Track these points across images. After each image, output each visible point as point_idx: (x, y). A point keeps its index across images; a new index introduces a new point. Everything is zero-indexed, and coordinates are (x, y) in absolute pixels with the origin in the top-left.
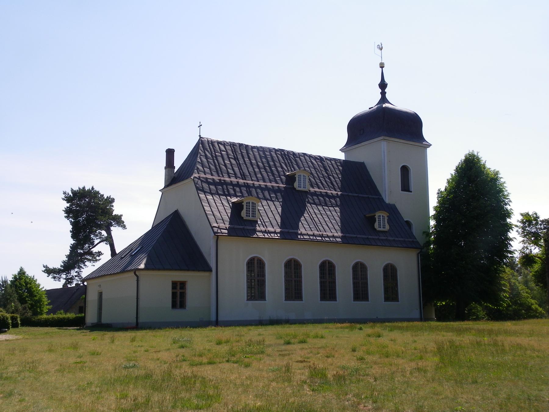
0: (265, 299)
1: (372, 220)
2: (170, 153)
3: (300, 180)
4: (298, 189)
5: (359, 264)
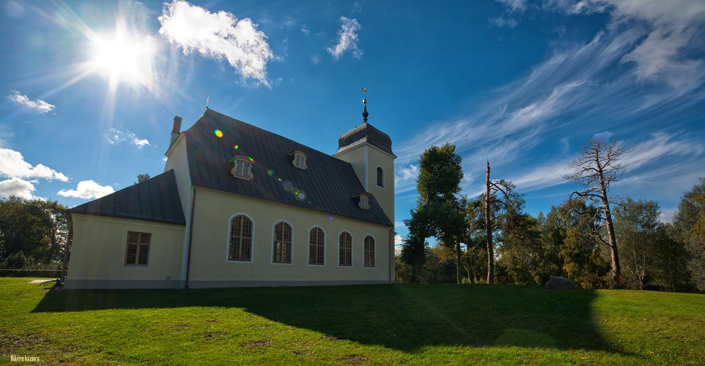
2: (178, 121)
3: (298, 160)
4: (296, 166)
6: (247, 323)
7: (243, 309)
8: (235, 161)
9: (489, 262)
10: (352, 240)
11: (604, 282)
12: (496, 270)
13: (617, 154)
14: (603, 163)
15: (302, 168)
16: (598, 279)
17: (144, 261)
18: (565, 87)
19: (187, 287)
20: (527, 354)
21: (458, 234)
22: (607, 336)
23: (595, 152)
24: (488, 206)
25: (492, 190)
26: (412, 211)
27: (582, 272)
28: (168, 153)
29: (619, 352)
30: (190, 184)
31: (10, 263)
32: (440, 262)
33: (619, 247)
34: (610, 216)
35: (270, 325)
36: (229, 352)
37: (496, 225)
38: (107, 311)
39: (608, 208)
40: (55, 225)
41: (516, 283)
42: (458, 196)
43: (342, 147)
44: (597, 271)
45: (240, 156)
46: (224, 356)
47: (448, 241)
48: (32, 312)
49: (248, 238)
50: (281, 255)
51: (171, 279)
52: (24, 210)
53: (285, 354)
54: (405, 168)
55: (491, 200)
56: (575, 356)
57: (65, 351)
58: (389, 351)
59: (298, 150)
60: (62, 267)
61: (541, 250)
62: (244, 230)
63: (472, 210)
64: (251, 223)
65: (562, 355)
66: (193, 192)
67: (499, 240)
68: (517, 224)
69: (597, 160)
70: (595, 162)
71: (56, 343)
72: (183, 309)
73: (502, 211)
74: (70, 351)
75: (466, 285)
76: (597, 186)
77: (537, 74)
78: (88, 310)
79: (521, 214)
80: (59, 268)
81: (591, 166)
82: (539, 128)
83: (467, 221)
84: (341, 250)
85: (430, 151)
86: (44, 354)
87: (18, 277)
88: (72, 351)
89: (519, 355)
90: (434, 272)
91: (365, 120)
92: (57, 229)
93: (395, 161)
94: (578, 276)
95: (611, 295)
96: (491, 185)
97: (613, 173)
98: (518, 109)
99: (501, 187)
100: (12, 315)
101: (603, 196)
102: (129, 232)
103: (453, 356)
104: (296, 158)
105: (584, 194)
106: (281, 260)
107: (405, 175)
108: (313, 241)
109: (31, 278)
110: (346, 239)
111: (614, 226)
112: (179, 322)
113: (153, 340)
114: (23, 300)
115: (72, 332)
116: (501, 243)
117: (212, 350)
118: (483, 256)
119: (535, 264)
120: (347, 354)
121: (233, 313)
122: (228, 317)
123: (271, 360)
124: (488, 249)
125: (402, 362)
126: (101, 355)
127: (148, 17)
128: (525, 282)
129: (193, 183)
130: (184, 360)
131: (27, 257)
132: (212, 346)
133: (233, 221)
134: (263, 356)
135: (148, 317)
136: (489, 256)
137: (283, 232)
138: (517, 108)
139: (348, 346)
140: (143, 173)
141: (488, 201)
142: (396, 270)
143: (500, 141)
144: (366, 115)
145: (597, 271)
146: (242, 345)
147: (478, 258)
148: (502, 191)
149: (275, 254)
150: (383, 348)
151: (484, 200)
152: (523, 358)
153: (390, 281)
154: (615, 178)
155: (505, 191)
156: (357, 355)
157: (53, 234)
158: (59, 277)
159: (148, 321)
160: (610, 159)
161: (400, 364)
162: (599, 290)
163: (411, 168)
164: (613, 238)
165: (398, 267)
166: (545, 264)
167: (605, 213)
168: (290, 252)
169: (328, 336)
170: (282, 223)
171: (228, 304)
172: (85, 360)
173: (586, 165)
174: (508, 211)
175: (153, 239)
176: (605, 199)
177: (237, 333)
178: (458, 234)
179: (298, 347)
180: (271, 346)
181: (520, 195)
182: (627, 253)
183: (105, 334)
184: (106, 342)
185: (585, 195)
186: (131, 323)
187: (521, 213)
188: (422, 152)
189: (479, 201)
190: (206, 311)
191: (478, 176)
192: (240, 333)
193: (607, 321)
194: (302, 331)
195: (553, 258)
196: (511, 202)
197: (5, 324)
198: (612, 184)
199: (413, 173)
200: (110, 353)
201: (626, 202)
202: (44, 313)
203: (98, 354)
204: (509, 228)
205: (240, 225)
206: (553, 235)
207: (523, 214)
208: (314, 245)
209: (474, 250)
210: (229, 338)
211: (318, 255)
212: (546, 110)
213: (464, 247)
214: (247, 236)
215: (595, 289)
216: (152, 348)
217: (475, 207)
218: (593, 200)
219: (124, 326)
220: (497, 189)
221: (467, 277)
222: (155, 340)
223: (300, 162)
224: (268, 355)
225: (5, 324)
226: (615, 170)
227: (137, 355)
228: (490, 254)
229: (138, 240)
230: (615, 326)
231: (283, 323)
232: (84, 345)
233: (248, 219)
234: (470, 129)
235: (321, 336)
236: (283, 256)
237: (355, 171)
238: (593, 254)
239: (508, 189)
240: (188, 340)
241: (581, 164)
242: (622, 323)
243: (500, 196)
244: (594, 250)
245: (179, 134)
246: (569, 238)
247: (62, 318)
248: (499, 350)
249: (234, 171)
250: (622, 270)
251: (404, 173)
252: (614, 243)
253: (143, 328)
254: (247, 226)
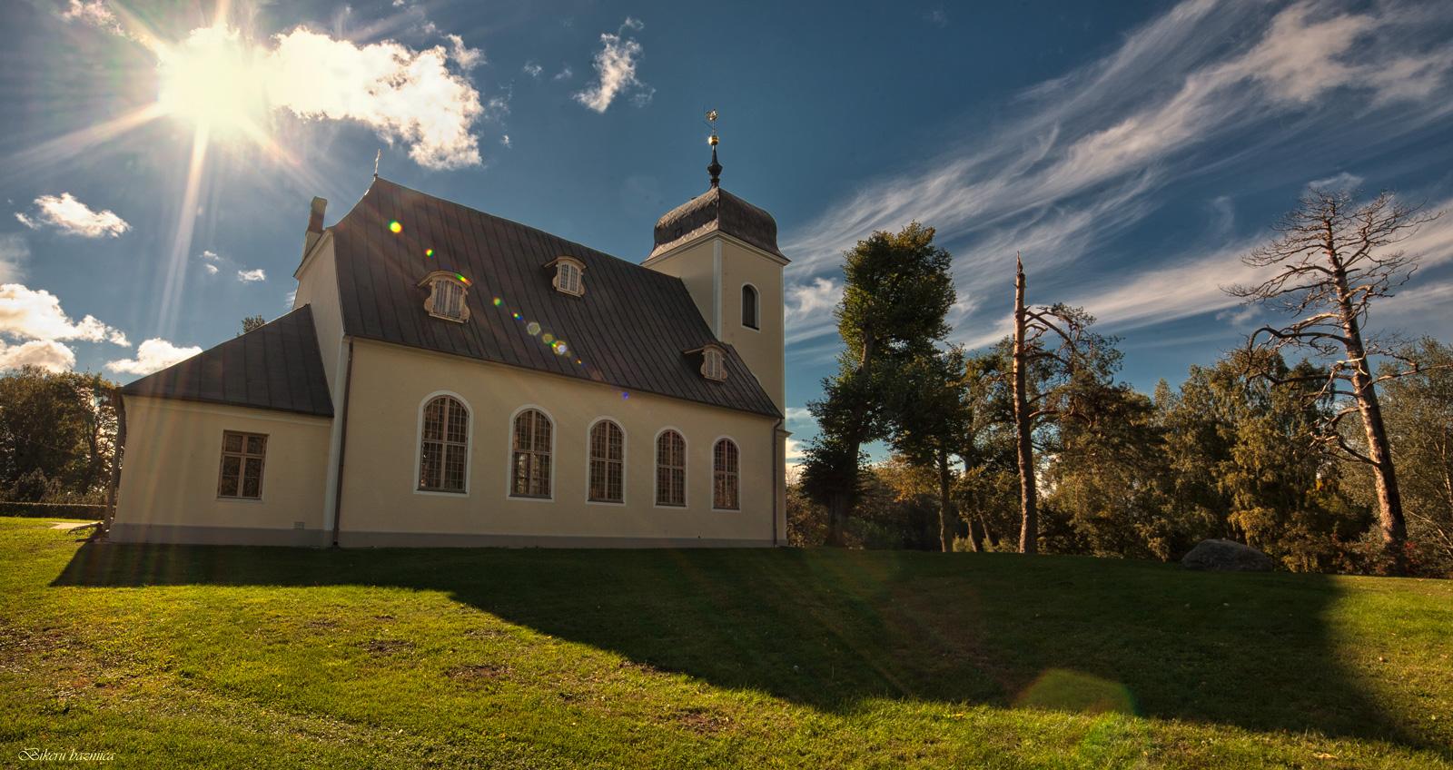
5: (726, 443)
6: (458, 625)
7: (449, 593)
8: (431, 284)
9: (1025, 500)
10: (739, 456)
11: (1356, 559)
12: (1044, 522)
13: (1389, 226)
14: (1346, 252)
15: (572, 293)
16: (1338, 549)
17: (253, 490)
18: (1218, 72)
19: (336, 543)
20: (1151, 734)
21: (943, 433)
22: (1390, 701)
23: (1324, 225)
24: (1021, 367)
25: (1031, 329)
26: (827, 381)
27: (1286, 531)
28: (299, 273)
29: (1433, 746)
30: (343, 334)
31: (23, 491)
32: (895, 501)
33: (1399, 467)
34: (1371, 386)
35: (506, 632)
36: (421, 687)
37: (1042, 413)
38: (183, 588)
39: (1364, 365)
40: (98, 419)
41: (1098, 554)
42: (943, 347)
43: (661, 243)
44: (1335, 529)
45: (441, 273)
46: (412, 694)
47: (916, 449)
48: (54, 584)
49: (458, 444)
50: (527, 479)
51: (306, 528)
52: (45, 391)
53: (541, 699)
54: (803, 287)
55: (1028, 355)
56: (1295, 750)
57: (106, 665)
58: (782, 706)
59: (564, 255)
60: (106, 498)
61: (1167, 476)
62: (450, 428)
63: (977, 379)
64: (464, 413)
65: (1255, 743)
66: (347, 350)
67: (1049, 447)
68: (1100, 410)
69: (1330, 246)
70: (1324, 250)
71: (91, 647)
72: (328, 589)
73: (1059, 381)
74: (115, 665)
75: (964, 554)
76: (1331, 313)
77: (1137, 47)
78: (150, 585)
79: (1110, 387)
80: (103, 502)
81: (1312, 261)
82: (1147, 177)
83: (966, 403)
84: (659, 470)
85: (870, 244)
86: (70, 669)
87: (33, 517)
88: (119, 666)
89: (1126, 736)
90: (883, 522)
91: (715, 182)
92: (99, 426)
93: (787, 271)
94: (1274, 540)
95: (1386, 593)
96: (1027, 317)
97: (1381, 278)
98: (1088, 136)
99: (1054, 320)
100: (20, 590)
101: (1348, 336)
102: (225, 431)
103: (945, 726)
104: (559, 272)
105: (1292, 332)
106: (527, 490)
107: (804, 302)
108: (597, 451)
109: (56, 519)
110: (671, 446)
111: (1383, 413)
112: (320, 616)
113: (268, 651)
114: (39, 560)
115: (121, 627)
116: (1054, 456)
117: (385, 681)
118: (1007, 488)
119: (1148, 506)
120: (682, 706)
121: (428, 603)
122: (418, 610)
123: (510, 711)
124: (1022, 471)
125: (815, 734)
126: (171, 677)
127: (258, 11)
128: (1121, 551)
129: (349, 332)
130: (330, 699)
131: (49, 480)
132: (386, 670)
133: (428, 408)
134: (492, 699)
135: (261, 603)
136: (1024, 487)
137: (532, 431)
138: (1087, 133)
139: (685, 687)
140: (253, 316)
141: (1020, 357)
142: (788, 517)
143: (1043, 212)
144: (715, 170)
145: (1335, 529)
146: (447, 673)
147: (993, 491)
148: (1058, 331)
149: (516, 478)
150: (768, 699)
151: (1010, 354)
152: (1140, 744)
153: (775, 541)
154: (1385, 290)
155: (1066, 330)
156: (707, 711)
157: (94, 437)
158: (102, 519)
159: (259, 611)
160: (1368, 242)
161: (810, 736)
162: (1343, 577)
163: (817, 286)
164: (1382, 442)
165: (793, 511)
166: (1175, 508)
167: (1355, 380)
168: (547, 475)
169: (636, 663)
170: (530, 413)
171: (418, 584)
172: (141, 685)
173: (1295, 260)
174: (1076, 379)
176: (1355, 344)
177: (437, 646)
178: (943, 433)
179: (568, 683)
180: (509, 678)
181: (1108, 341)
182: (1424, 482)
183: (180, 635)
184: (181, 652)
185: (1293, 336)
186: (227, 615)
187: (1110, 383)
188: (851, 247)
189: (994, 357)
190: (372, 595)
191: (985, 298)
192: (444, 646)
193: (1385, 661)
194: (576, 649)
195: (1199, 492)
196: (1081, 356)
197: (8, 606)
198: (1376, 304)
199: (823, 296)
200: (187, 675)
201: (1420, 350)
202: (74, 589)
203: (166, 675)
204: (1075, 423)
205: (442, 418)
206: (1199, 438)
207: (1116, 384)
208: (601, 459)
209: (983, 474)
210: (421, 656)
211: (610, 482)
212: (1165, 132)
213: (957, 465)
214: (456, 440)
215: (1325, 572)
216: (266, 668)
217: (986, 371)
218: (1316, 347)
219: (214, 620)
220: (1044, 326)
221: (964, 535)
222: (273, 652)
223: (569, 279)
224: (504, 697)
225: (8, 606)
226: (1385, 270)
227: (237, 681)
228: (1026, 483)
229: (243, 448)
230: (1411, 675)
231: (534, 629)
232: (139, 654)
234: (962, 191)
235: (619, 662)
236: (533, 483)
237: (691, 295)
238: (1319, 485)
239: (1074, 325)
240: (337, 656)
241: (1278, 258)
242: (1433, 667)
243: (1051, 342)
244: (1318, 476)
245: (321, 232)
246: (1245, 443)
247: (104, 598)
248: (1070, 719)
249: (429, 304)
250: (1412, 527)
251: (799, 297)
252: (1385, 456)
253: (251, 625)
254: (457, 419)
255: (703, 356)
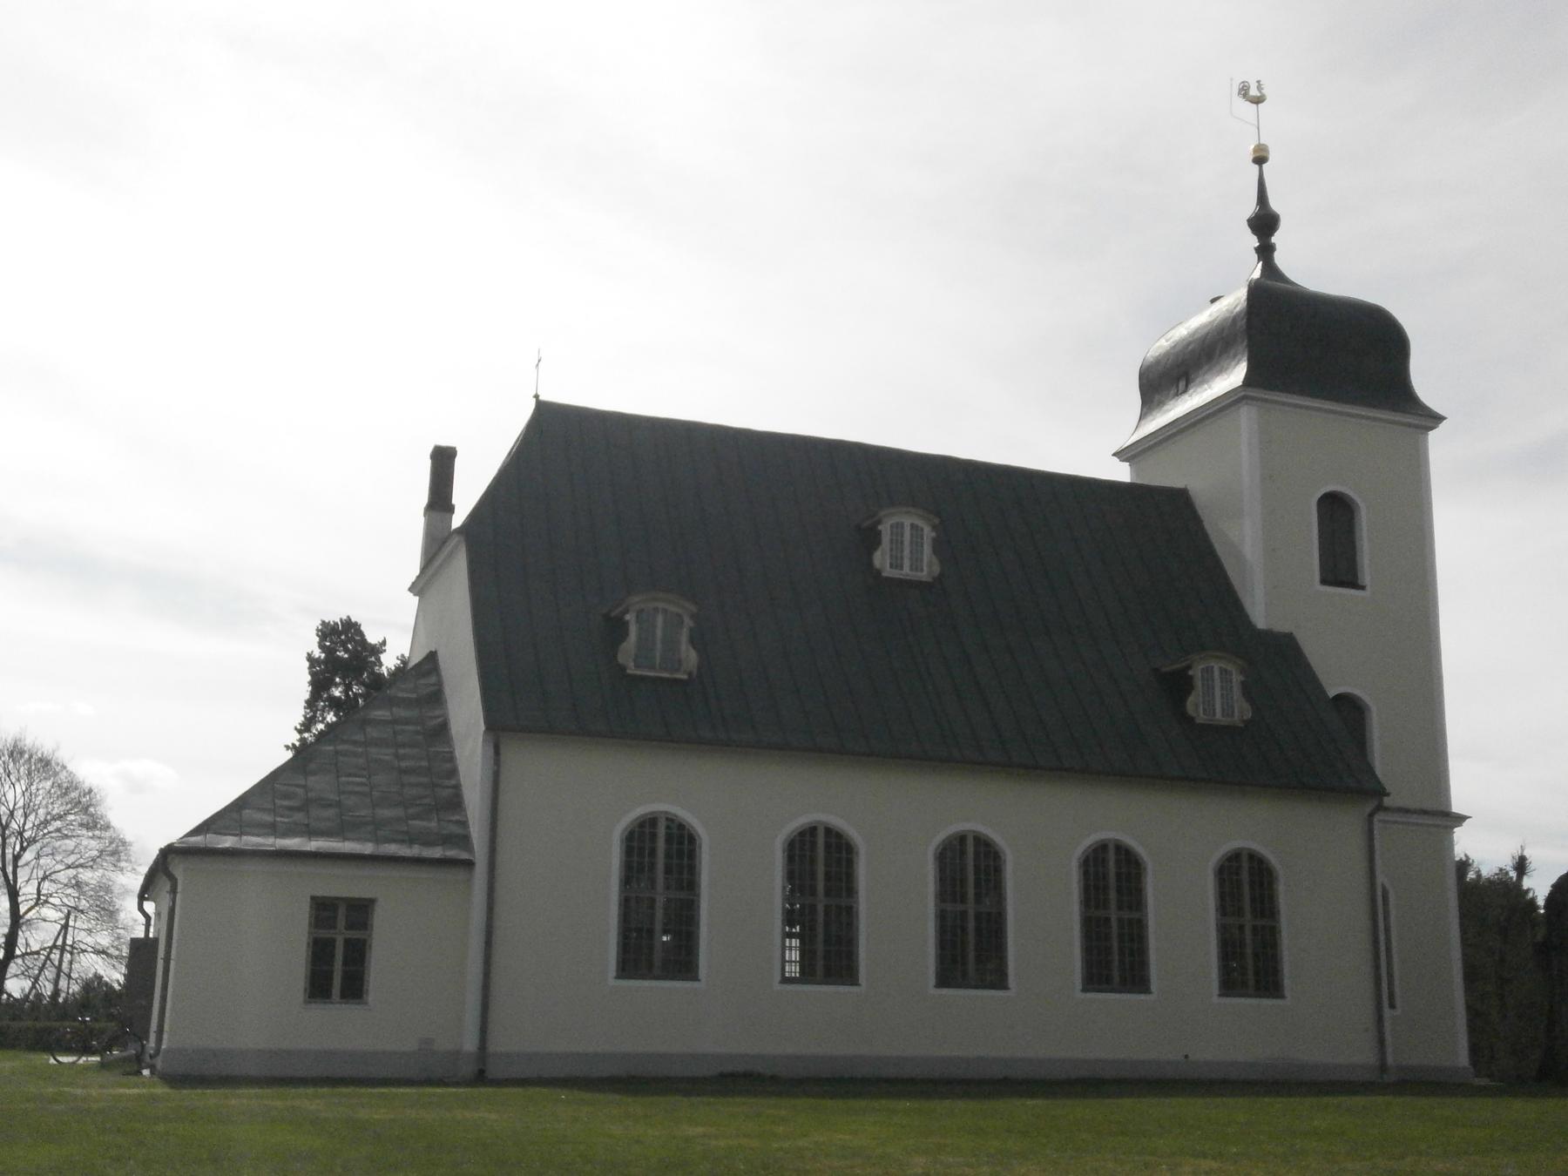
0: (697, 972)
1: (1178, 686)
2: (443, 461)
3: (897, 542)
4: (888, 572)
5: (1245, 858)
8: (628, 617)
30: (483, 728)
64: (692, 839)
153: (1383, 1068)
175: (381, 920)
233: (681, 826)
255: (1191, 678)
